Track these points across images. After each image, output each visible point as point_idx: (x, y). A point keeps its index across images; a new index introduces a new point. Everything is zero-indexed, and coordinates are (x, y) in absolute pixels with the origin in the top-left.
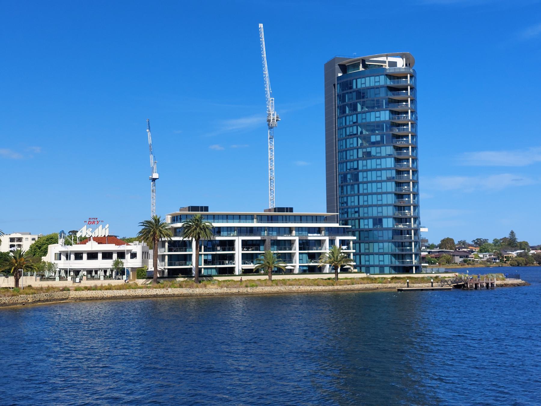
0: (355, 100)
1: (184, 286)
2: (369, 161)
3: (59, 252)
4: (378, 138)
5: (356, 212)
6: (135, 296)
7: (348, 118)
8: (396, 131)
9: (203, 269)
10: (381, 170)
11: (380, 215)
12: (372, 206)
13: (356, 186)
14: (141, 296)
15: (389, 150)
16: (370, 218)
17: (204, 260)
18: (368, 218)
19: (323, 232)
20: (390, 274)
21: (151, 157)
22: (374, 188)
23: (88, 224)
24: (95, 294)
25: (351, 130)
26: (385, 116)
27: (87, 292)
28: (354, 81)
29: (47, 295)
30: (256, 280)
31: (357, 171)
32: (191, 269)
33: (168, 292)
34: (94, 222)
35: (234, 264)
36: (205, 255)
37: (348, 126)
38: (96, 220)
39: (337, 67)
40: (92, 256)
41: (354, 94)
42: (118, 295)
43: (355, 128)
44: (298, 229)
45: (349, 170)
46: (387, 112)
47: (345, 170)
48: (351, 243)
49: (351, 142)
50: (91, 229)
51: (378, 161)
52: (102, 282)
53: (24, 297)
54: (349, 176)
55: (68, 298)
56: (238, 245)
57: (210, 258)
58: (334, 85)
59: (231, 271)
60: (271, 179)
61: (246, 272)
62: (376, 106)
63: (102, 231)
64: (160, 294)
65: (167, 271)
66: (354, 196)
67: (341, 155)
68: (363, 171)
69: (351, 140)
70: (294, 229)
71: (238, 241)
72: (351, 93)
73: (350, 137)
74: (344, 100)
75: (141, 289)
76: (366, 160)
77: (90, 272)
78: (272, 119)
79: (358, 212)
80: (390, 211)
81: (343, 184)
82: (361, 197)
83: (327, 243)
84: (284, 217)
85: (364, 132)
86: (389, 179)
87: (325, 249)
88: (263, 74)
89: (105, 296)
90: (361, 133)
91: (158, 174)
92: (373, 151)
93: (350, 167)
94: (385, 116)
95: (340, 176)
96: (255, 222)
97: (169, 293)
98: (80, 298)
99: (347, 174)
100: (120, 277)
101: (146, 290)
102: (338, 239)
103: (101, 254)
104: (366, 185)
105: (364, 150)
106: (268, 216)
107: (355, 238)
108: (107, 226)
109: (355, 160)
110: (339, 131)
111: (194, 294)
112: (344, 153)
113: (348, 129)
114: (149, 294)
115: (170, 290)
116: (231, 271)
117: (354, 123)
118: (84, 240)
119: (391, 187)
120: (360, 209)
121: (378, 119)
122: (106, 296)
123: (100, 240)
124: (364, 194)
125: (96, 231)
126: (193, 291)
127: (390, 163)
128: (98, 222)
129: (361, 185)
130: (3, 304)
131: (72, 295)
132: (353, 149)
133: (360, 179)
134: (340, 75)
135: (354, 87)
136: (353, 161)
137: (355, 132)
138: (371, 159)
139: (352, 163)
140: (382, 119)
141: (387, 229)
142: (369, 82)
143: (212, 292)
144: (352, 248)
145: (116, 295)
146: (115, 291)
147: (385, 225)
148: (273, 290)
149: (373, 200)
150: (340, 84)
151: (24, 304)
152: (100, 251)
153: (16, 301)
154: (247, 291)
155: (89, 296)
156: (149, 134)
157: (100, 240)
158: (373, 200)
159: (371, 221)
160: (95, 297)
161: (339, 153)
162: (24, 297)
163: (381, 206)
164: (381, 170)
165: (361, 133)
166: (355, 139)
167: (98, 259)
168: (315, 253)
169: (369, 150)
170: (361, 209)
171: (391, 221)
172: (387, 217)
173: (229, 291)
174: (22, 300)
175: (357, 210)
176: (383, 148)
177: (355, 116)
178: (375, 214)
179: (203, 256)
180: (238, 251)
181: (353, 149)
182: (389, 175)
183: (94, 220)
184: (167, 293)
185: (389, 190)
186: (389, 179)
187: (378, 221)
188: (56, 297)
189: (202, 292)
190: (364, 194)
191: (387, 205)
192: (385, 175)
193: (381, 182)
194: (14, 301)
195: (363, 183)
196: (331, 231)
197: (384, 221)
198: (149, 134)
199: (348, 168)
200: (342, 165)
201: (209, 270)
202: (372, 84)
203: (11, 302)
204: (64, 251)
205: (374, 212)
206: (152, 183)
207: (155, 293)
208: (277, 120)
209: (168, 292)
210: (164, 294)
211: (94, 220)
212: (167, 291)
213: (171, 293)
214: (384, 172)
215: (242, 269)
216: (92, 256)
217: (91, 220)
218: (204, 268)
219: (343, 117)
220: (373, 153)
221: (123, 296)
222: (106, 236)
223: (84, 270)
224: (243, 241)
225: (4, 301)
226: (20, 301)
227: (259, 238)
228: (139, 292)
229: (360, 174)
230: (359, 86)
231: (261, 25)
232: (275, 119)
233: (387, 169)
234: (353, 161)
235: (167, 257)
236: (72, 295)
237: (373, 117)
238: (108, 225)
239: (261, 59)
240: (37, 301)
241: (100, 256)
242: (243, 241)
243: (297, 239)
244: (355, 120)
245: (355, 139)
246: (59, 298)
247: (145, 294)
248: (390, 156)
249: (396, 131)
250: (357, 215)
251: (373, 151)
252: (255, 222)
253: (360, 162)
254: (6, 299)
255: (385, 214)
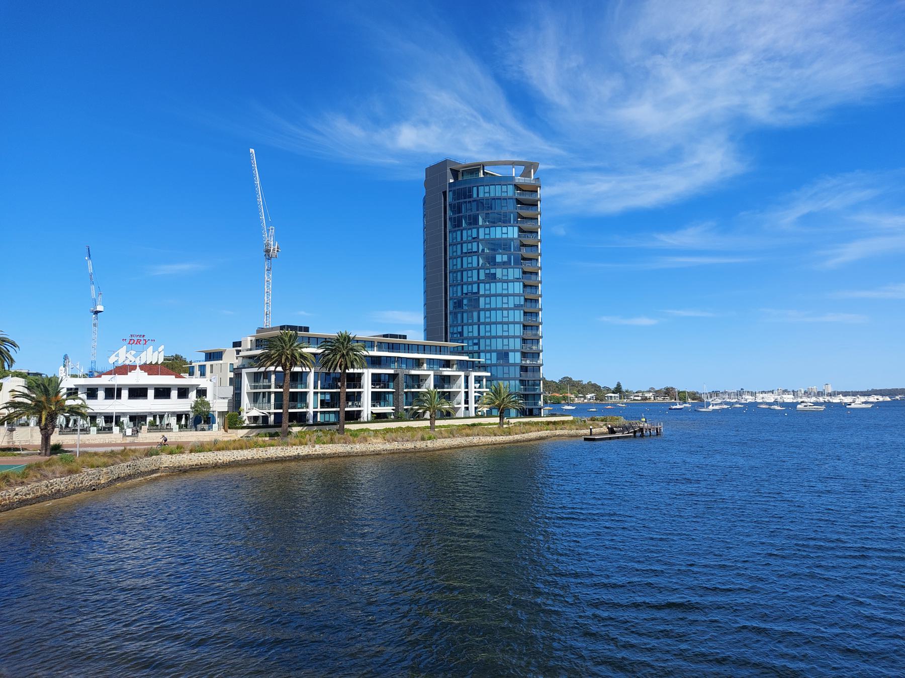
0: (474, 212)
1: (336, 441)
2: (493, 285)
3: (74, 387)
4: (505, 258)
5: (475, 344)
6: (267, 459)
7: (465, 232)
8: (524, 252)
9: (319, 414)
10: (507, 295)
11: (506, 348)
12: (496, 337)
13: (459, 316)
14: (276, 458)
15: (515, 273)
16: (494, 351)
17: (321, 400)
18: (491, 351)
19: (455, 366)
20: (517, 417)
21: (93, 287)
22: (498, 316)
23: (129, 343)
24: (203, 458)
25: (470, 247)
26: (513, 232)
27: (190, 455)
28: (475, 189)
29: (130, 466)
30: (371, 430)
31: (478, 295)
32: (305, 413)
33: (316, 451)
34: (139, 342)
35: (360, 407)
36: (321, 393)
37: (465, 242)
38: (142, 339)
39: (449, 171)
40: (138, 392)
41: (474, 204)
42: (240, 458)
43: (475, 244)
44: (430, 361)
45: (466, 294)
46: (516, 229)
47: (459, 294)
48: (484, 380)
49: (455, 263)
50: (133, 352)
51: (505, 285)
52: (176, 435)
53: (93, 474)
54: (465, 302)
55: (159, 469)
56: (367, 380)
57: (328, 397)
58: (445, 193)
59: (354, 417)
60: (267, 314)
61: (379, 417)
62: (504, 221)
63: (154, 356)
64: (304, 454)
65: (272, 417)
66: (472, 324)
67: (453, 277)
68: (485, 296)
69: (470, 259)
70: (425, 361)
71: (367, 374)
72: (470, 202)
73: (468, 255)
74: (460, 211)
75: (275, 448)
76: (489, 283)
77: (108, 418)
78: (272, 249)
79: (478, 344)
80: (518, 343)
81: (457, 311)
82: (482, 327)
83: (462, 380)
84: (407, 346)
85: (487, 251)
86: (517, 307)
87: (460, 388)
88: (257, 201)
89: (219, 461)
90: (483, 250)
91: (103, 307)
92: (499, 272)
93: (468, 290)
94: (513, 232)
95: (451, 301)
96: (375, 350)
97: (316, 453)
98: (179, 467)
99: (463, 299)
100: (206, 426)
101: (282, 449)
102: (473, 375)
103: (153, 391)
104: (489, 312)
105: (487, 271)
106: (389, 343)
107: (489, 374)
108: (163, 347)
109: (475, 283)
110: (451, 247)
111: (353, 452)
112: (459, 274)
113: (465, 245)
114: (287, 455)
115: (317, 447)
116: (354, 417)
117: (474, 238)
118: (123, 370)
119: (518, 316)
120: (481, 340)
121: (504, 236)
122: (221, 461)
123: (150, 369)
124: (485, 324)
125: (143, 355)
126: (352, 448)
127: (518, 288)
128: (146, 342)
129: (482, 313)
130: (56, 493)
131: (165, 462)
132: (472, 269)
133: (482, 305)
134: (451, 181)
135: (475, 195)
136: (472, 283)
137: (475, 249)
138: (496, 282)
139: (470, 287)
140: (510, 236)
141: (515, 365)
142: (496, 191)
143: (379, 449)
144: (484, 387)
145: (237, 459)
146: (235, 451)
147: (511, 361)
148: (453, 444)
149: (499, 330)
150: (454, 191)
151: (94, 490)
152: (151, 386)
153: (79, 484)
154: (426, 446)
155: (194, 463)
156: (90, 263)
157: (150, 369)
158: (499, 330)
159: (494, 355)
160: (204, 464)
161: (451, 274)
162: (93, 474)
163: (508, 337)
164: (507, 295)
165: (483, 250)
166: (475, 258)
167: (170, 398)
168: (297, 392)
169: (493, 271)
170: (482, 341)
171: (518, 355)
172: (514, 351)
173: (401, 447)
174: (91, 480)
175: (476, 341)
176: (511, 271)
177: (475, 231)
178: (500, 347)
179: (319, 394)
180: (367, 389)
181: (472, 269)
182: (517, 303)
183: (138, 338)
184: (313, 453)
185: (517, 320)
186: (517, 307)
187: (504, 355)
188: (143, 469)
189: (364, 449)
190: (485, 324)
191: (514, 337)
192: (512, 302)
193: (508, 309)
194: (75, 484)
195: (485, 310)
196: (462, 365)
197: (511, 355)
198: (90, 263)
199: (465, 291)
200: (455, 288)
201: (327, 416)
202: (498, 194)
203: (71, 487)
204: (83, 385)
205: (499, 345)
206: (94, 316)
207: (296, 453)
208: (278, 251)
209: (316, 451)
210: (310, 455)
211: (138, 338)
212: (314, 449)
213: (320, 453)
214: (511, 298)
215: (372, 412)
216: (138, 392)
217: (133, 338)
218: (321, 412)
219: (458, 230)
220: (499, 275)
221: (248, 460)
222: (159, 363)
223: (151, 414)
224: (373, 374)
225: (58, 487)
226: (86, 483)
227: (391, 371)
228: (272, 452)
229: (482, 300)
230: (481, 195)
231: (252, 150)
232: (276, 249)
233: (514, 295)
234: (472, 283)
235: (273, 396)
236: (165, 462)
237: (498, 233)
238: (163, 346)
239: (254, 186)
240: (115, 480)
241: (151, 393)
242: (373, 374)
243: (431, 373)
244: (474, 235)
245: (475, 258)
246: (146, 470)
247: (281, 456)
248: (518, 280)
249: (524, 252)
250: (476, 348)
251: (499, 272)
252: (375, 350)
253: (482, 285)
254: (62, 483)
255: (512, 347)
